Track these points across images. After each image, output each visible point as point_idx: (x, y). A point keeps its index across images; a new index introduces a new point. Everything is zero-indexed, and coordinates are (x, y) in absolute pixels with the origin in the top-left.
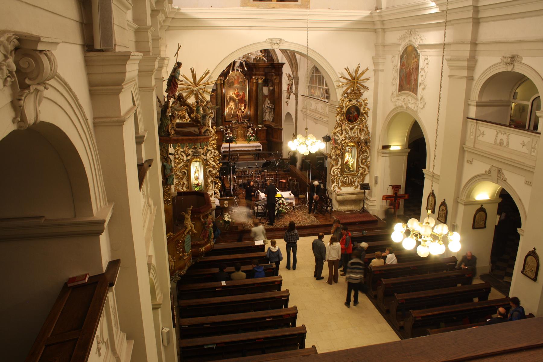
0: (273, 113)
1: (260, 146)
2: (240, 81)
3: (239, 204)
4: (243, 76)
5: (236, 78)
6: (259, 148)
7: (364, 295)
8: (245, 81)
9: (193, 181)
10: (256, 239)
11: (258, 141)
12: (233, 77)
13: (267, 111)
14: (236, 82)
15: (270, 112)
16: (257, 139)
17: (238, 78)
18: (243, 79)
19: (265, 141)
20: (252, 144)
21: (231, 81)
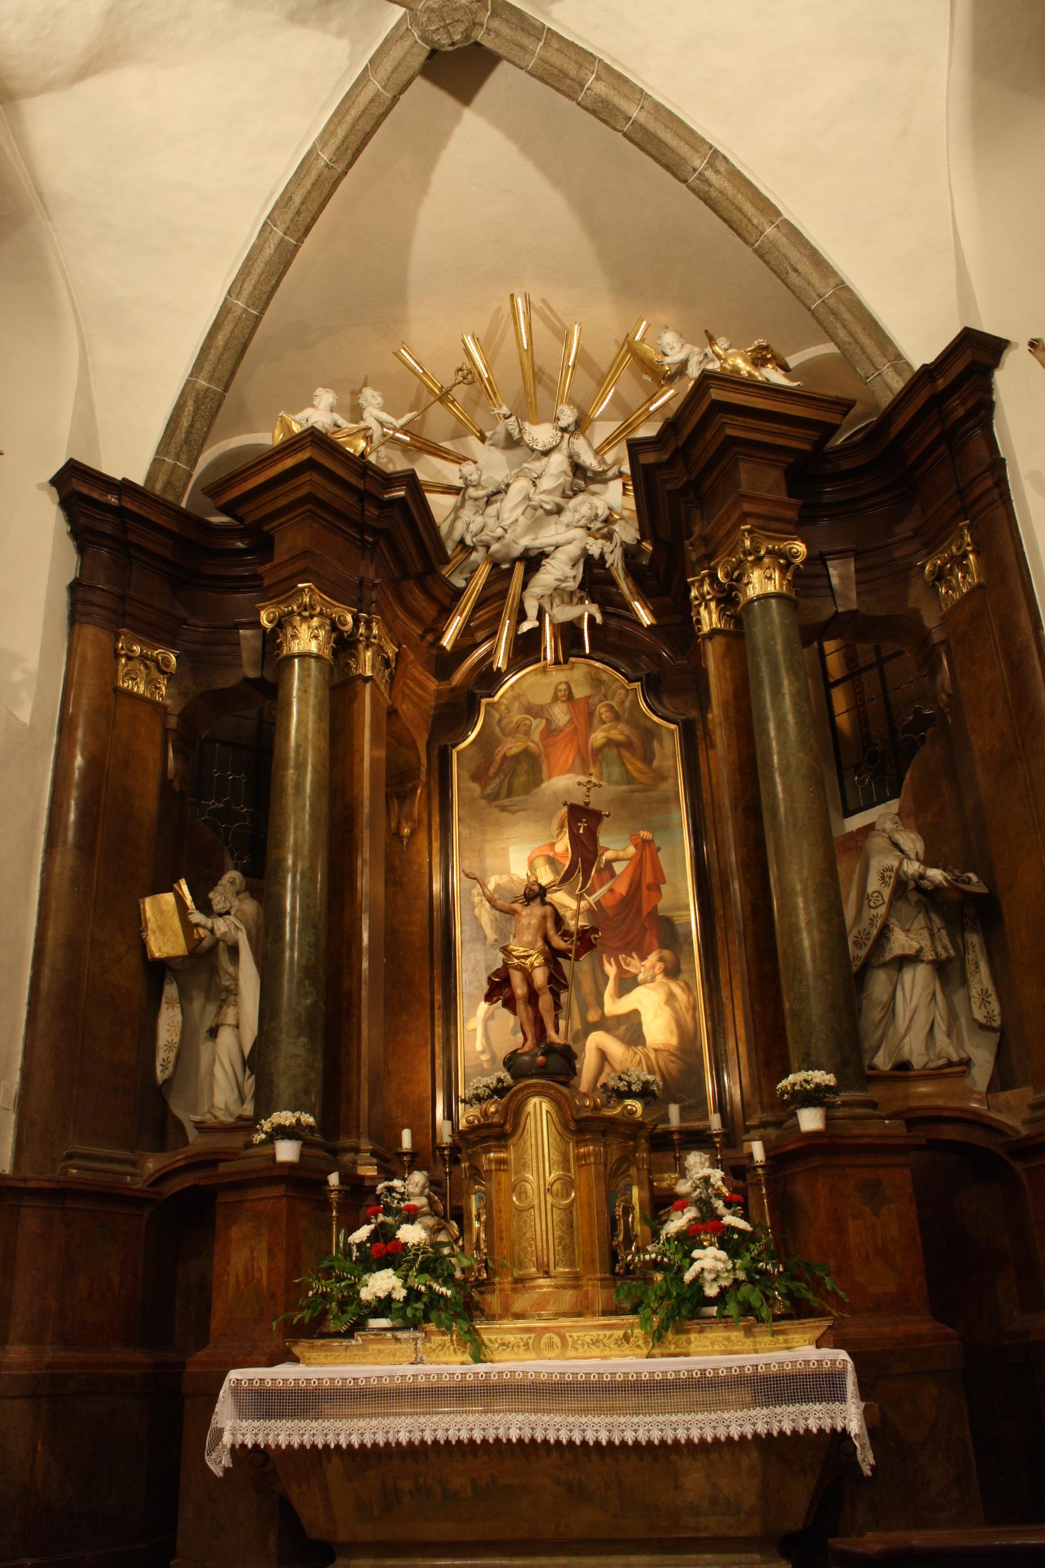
0: (981, 978)
1: (822, 1386)
2: (598, 737)
3: (417, 1247)
4: (624, 690)
5: (560, 714)
6: (813, 1417)
7: (993, 380)
8: (649, 734)
9: (175, 986)
10: (493, 1301)
11: (799, 1310)
12: (534, 711)
13: (901, 942)
14: (566, 755)
15: (948, 972)
16: (785, 1286)
17: (585, 715)
18: (634, 718)
19: (923, 1325)
20: (714, 1351)
21: (512, 747)
